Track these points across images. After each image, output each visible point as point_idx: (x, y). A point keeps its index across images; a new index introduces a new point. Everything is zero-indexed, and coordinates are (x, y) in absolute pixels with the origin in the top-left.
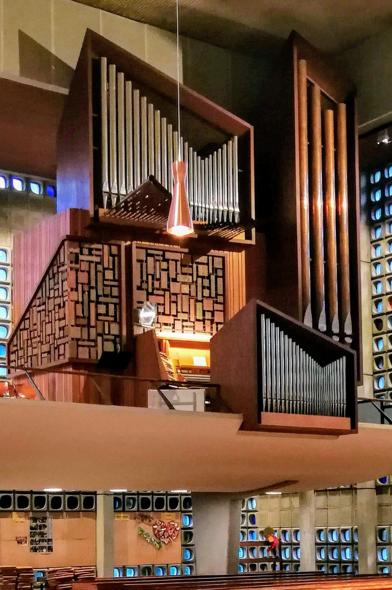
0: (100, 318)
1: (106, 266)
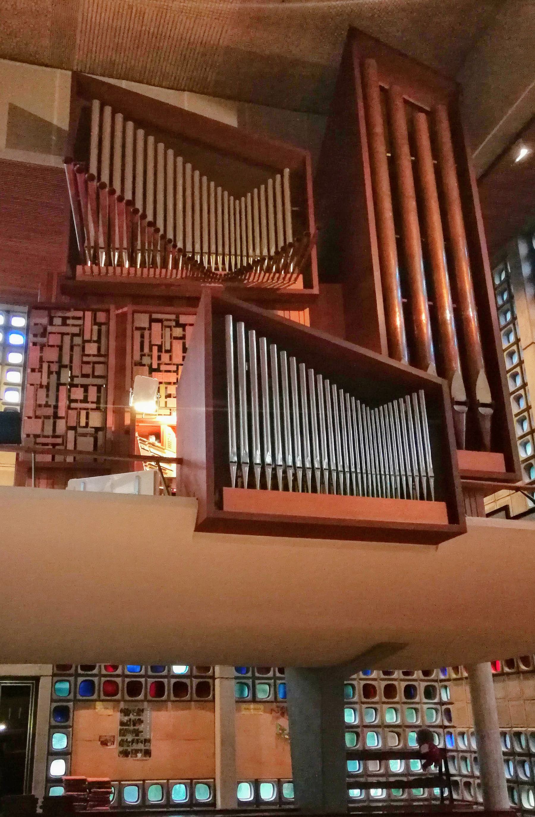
0: (73, 405)
1: (87, 337)
